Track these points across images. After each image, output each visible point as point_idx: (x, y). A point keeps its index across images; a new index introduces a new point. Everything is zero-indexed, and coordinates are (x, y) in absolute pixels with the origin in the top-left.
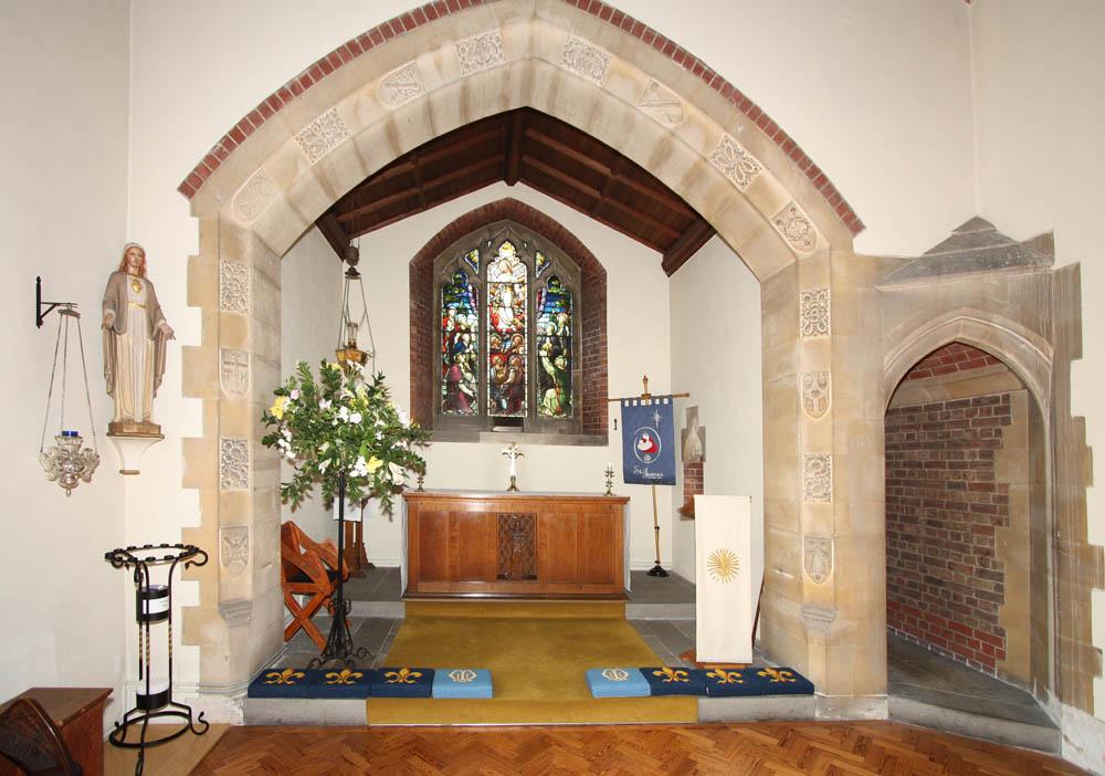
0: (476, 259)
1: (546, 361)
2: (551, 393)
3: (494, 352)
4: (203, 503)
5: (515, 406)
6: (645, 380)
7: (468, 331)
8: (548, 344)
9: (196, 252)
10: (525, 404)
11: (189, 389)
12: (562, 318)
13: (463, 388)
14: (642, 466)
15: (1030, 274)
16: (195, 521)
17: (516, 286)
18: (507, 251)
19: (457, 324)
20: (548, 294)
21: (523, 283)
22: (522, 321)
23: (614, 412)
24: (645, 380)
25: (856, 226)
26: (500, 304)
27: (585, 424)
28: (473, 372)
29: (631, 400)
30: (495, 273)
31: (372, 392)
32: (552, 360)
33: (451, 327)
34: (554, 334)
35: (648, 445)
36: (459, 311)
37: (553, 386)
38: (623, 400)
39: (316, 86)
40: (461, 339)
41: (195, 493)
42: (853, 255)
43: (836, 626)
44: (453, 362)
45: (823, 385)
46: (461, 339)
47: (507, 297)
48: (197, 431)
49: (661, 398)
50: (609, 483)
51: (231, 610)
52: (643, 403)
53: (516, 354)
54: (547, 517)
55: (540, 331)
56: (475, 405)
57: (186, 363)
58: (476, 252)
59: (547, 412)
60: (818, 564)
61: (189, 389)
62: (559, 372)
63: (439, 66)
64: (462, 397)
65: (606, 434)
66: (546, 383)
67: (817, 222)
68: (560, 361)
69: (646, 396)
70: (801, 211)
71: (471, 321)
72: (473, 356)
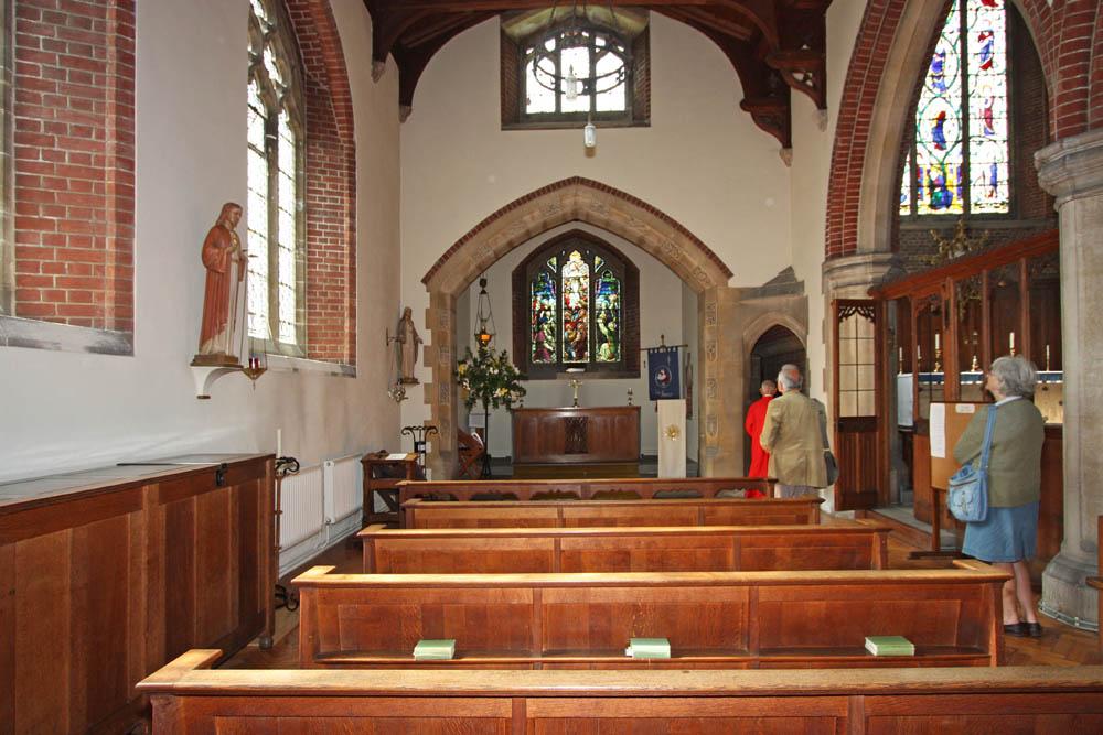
0: (555, 263)
1: (602, 326)
2: (605, 346)
3: (567, 322)
4: (433, 410)
5: (581, 356)
6: (662, 337)
7: (549, 309)
8: (603, 315)
9: (428, 306)
10: (588, 353)
11: (426, 364)
12: (612, 297)
13: (547, 345)
14: (660, 389)
15: (796, 297)
16: (429, 418)
17: (582, 280)
18: (575, 257)
19: (542, 305)
20: (603, 283)
21: (586, 277)
22: (586, 301)
23: (644, 356)
24: (662, 337)
25: (729, 275)
26: (571, 291)
27: (626, 366)
28: (553, 335)
29: (654, 349)
30: (567, 271)
31: (501, 359)
32: (606, 325)
33: (538, 307)
34: (607, 308)
35: (664, 377)
36: (544, 297)
37: (606, 341)
38: (649, 350)
39: (479, 233)
40: (545, 315)
41: (430, 406)
42: (728, 288)
43: (718, 455)
44: (540, 330)
45: (714, 347)
46: (545, 315)
47: (575, 286)
48: (430, 381)
49: (672, 348)
50: (630, 399)
51: (443, 454)
52: (661, 351)
53: (582, 322)
54: (598, 419)
55: (597, 307)
56: (554, 356)
57: (425, 351)
58: (555, 259)
59: (603, 358)
60: (712, 429)
61: (426, 364)
62: (610, 332)
63: (533, 218)
64: (545, 351)
65: (639, 370)
66: (603, 340)
67: (711, 272)
68: (611, 325)
69: (663, 347)
70: (702, 269)
71: (552, 302)
72: (553, 325)
